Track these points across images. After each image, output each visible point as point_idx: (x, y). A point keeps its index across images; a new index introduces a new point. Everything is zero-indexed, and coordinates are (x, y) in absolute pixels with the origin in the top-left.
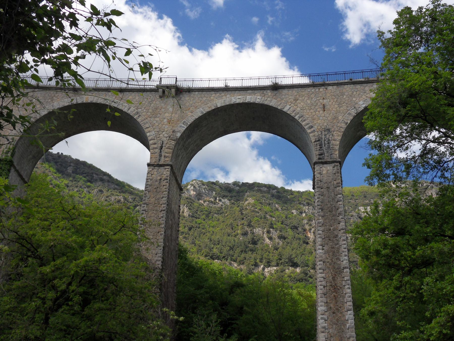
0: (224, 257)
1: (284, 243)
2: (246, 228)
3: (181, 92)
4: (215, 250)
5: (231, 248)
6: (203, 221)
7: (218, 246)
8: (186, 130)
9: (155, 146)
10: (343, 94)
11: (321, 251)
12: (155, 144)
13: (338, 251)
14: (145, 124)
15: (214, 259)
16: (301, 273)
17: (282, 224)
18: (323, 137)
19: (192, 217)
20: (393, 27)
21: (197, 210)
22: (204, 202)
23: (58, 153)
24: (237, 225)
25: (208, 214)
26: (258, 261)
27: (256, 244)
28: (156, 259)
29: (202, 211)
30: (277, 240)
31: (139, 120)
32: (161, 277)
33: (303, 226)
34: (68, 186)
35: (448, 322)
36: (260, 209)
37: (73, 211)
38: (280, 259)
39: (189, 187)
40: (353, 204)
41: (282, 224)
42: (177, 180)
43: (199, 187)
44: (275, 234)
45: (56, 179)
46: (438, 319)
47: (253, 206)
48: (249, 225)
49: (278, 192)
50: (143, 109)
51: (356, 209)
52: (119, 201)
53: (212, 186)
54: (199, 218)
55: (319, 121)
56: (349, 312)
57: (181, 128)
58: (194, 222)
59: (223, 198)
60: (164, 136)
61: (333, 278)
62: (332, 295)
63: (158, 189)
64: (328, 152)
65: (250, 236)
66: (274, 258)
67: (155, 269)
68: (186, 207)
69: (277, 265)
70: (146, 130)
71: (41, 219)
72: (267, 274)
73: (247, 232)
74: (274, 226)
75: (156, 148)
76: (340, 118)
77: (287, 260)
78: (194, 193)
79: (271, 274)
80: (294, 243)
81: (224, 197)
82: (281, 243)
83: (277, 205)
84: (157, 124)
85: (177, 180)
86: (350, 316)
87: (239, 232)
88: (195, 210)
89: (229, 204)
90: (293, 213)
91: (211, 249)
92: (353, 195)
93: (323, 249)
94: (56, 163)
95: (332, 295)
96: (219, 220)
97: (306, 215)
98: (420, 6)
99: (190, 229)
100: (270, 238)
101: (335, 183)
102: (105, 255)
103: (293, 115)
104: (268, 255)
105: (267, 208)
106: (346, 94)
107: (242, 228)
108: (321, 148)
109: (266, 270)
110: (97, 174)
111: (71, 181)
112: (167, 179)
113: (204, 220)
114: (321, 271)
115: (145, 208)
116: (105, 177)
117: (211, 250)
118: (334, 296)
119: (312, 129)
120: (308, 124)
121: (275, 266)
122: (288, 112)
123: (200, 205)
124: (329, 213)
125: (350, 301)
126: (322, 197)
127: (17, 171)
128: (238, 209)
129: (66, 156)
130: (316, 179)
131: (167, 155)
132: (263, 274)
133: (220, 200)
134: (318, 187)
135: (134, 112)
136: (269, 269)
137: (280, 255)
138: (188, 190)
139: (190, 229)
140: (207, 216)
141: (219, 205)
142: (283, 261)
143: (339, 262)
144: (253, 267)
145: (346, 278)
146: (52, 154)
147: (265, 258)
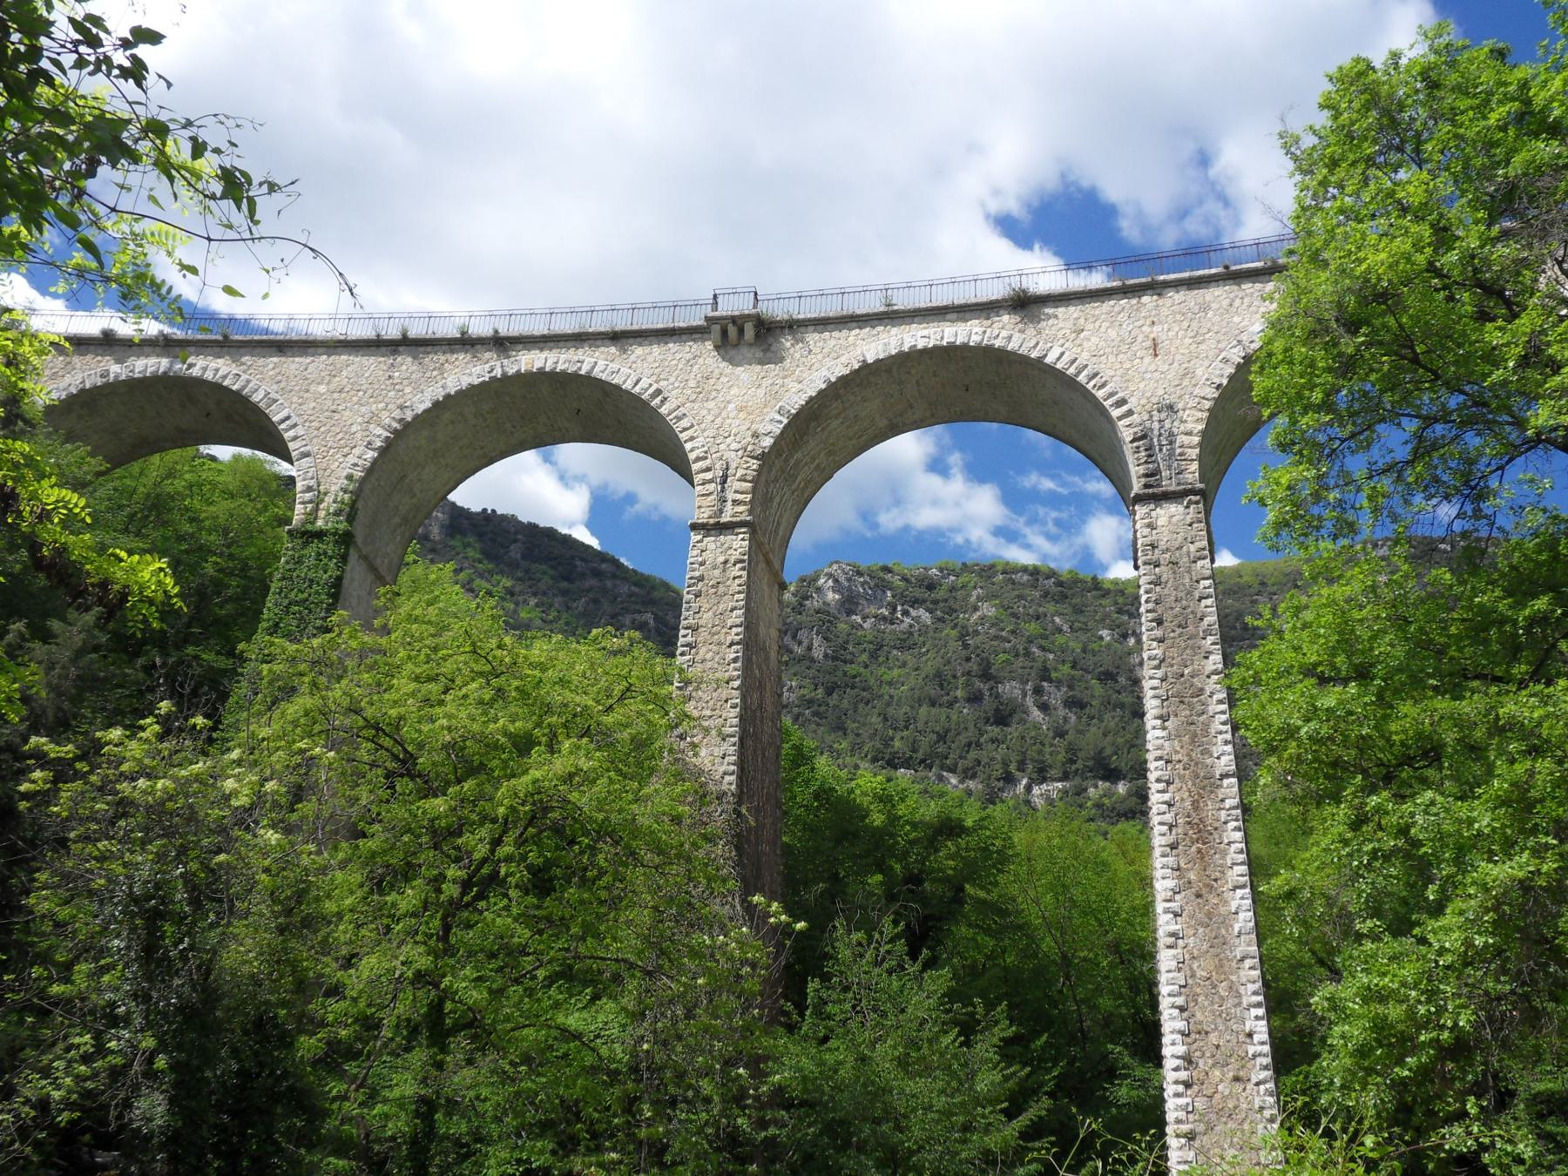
0: (923, 761)
1: (1080, 718)
2: (978, 684)
3: (769, 330)
4: (897, 744)
5: (942, 738)
7: (906, 733)
8: (786, 427)
9: (709, 476)
11: (1159, 733)
12: (708, 469)
13: (1206, 732)
14: (679, 419)
15: (896, 768)
16: (1129, 794)
17: (1073, 667)
19: (835, 659)
20: (1323, 119)
21: (847, 642)
22: (864, 618)
23: (485, 510)
24: (954, 677)
25: (877, 649)
26: (1013, 768)
27: (1007, 725)
28: (722, 769)
30: (1062, 712)
31: (663, 411)
32: (739, 814)
33: (1131, 671)
34: (512, 594)
35: (1487, 910)
36: (1013, 632)
37: (499, 653)
38: (1073, 762)
39: (822, 581)
41: (1073, 667)
42: (768, 563)
43: (849, 580)
44: (1056, 697)
45: (481, 576)
46: (1459, 904)
48: (986, 676)
49: (1060, 584)
50: (672, 379)
55: (1142, 385)
56: (1239, 892)
57: (771, 426)
58: (839, 673)
61: (1196, 805)
62: (1194, 849)
63: (721, 589)
64: (1169, 467)
65: (988, 704)
66: (1056, 754)
67: (721, 797)
69: (1065, 777)
70: (683, 436)
71: (417, 679)
72: (1039, 802)
73: (982, 694)
74: (1054, 675)
75: (711, 481)
76: (1199, 372)
77: (1091, 763)
79: (1050, 801)
80: (1107, 716)
81: (916, 603)
82: (1074, 718)
83: (1057, 620)
84: (710, 418)
85: (768, 563)
86: (1240, 901)
87: (959, 693)
90: (1101, 638)
91: (887, 742)
92: (1263, 584)
93: (1164, 729)
94: (480, 536)
95: (1194, 849)
96: (904, 665)
98: (1394, 48)
99: (829, 692)
100: (1044, 707)
101: (1192, 548)
102: (585, 765)
104: (1040, 752)
105: (1032, 628)
106: (1214, 306)
107: (967, 684)
108: (1150, 456)
109: (1036, 790)
110: (583, 560)
111: (519, 579)
112: (742, 561)
113: (866, 667)
114: (1161, 786)
115: (689, 639)
116: (604, 566)
117: (887, 745)
118: (1199, 851)
119: (1125, 408)
121: (1060, 780)
122: (1059, 366)
124: (1179, 631)
125: (1242, 863)
126: (1158, 589)
127: (365, 558)
128: (954, 633)
129: (504, 517)
130: (1139, 542)
131: (739, 497)
132: (1028, 802)
133: (906, 613)
134: (1145, 563)
135: (651, 391)
136: (1044, 787)
137: (1072, 750)
138: (819, 590)
139: (829, 692)
140: (874, 655)
141: (904, 626)
142: (1080, 765)
143: (1209, 761)
144: (1001, 784)
145: (1229, 803)
146: (459, 513)
147: (1032, 760)
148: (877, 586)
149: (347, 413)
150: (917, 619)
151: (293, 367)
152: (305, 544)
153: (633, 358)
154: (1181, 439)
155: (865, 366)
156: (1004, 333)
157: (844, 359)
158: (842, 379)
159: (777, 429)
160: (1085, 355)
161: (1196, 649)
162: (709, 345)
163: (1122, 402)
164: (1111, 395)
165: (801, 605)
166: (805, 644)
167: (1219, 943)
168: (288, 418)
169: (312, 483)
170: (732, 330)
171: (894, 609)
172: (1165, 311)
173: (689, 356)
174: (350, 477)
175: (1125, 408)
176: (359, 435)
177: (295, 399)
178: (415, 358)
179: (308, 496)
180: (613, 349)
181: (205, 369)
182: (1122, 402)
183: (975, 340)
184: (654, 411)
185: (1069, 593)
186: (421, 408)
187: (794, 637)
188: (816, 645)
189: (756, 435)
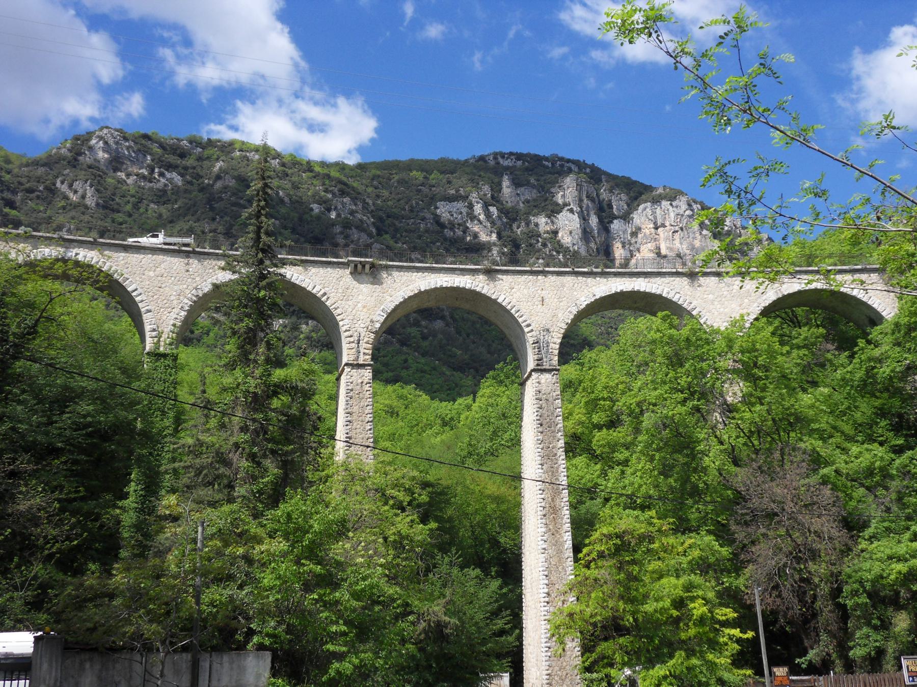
6: (127, 219)
9: (352, 339)
10: (563, 286)
12: (351, 336)
18: (542, 338)
21: (114, 194)
22: (128, 175)
29: (124, 196)
31: (328, 303)
33: (333, 238)
40: (426, 196)
43: (117, 143)
47: (234, 194)
49: (283, 165)
51: (430, 205)
53: (143, 142)
54: (119, 212)
59: (167, 170)
61: (553, 499)
68: (91, 186)
70: (338, 318)
76: (560, 315)
78: (106, 156)
81: (170, 167)
88: (109, 193)
89: (180, 183)
90: (312, 210)
97: (338, 215)
103: (509, 307)
119: (530, 328)
120: (525, 321)
123: (119, 182)
131: (367, 351)
133: (161, 175)
138: (91, 148)
141: (160, 185)
148: (139, 150)
149: (167, 289)
150: (170, 180)
151: (134, 259)
152: (157, 361)
153: (310, 273)
154: (552, 345)
155: (420, 293)
156: (481, 285)
157: (410, 287)
158: (410, 297)
159: (382, 319)
160: (514, 300)
161: (554, 437)
162: (348, 271)
163: (529, 325)
164: (525, 321)
165: (76, 160)
166: (80, 193)
167: (560, 552)
168: (136, 290)
169: (155, 327)
170: (359, 266)
171: (152, 171)
172: (547, 285)
173: (338, 276)
174: (174, 325)
175: (530, 328)
176: (175, 302)
177: (138, 279)
178: (199, 261)
179: (154, 334)
180: (300, 268)
181: (77, 254)
182: (529, 325)
183: (468, 286)
184: (323, 303)
185: (290, 172)
186: (206, 290)
187: (70, 186)
188: (89, 195)
189: (372, 321)
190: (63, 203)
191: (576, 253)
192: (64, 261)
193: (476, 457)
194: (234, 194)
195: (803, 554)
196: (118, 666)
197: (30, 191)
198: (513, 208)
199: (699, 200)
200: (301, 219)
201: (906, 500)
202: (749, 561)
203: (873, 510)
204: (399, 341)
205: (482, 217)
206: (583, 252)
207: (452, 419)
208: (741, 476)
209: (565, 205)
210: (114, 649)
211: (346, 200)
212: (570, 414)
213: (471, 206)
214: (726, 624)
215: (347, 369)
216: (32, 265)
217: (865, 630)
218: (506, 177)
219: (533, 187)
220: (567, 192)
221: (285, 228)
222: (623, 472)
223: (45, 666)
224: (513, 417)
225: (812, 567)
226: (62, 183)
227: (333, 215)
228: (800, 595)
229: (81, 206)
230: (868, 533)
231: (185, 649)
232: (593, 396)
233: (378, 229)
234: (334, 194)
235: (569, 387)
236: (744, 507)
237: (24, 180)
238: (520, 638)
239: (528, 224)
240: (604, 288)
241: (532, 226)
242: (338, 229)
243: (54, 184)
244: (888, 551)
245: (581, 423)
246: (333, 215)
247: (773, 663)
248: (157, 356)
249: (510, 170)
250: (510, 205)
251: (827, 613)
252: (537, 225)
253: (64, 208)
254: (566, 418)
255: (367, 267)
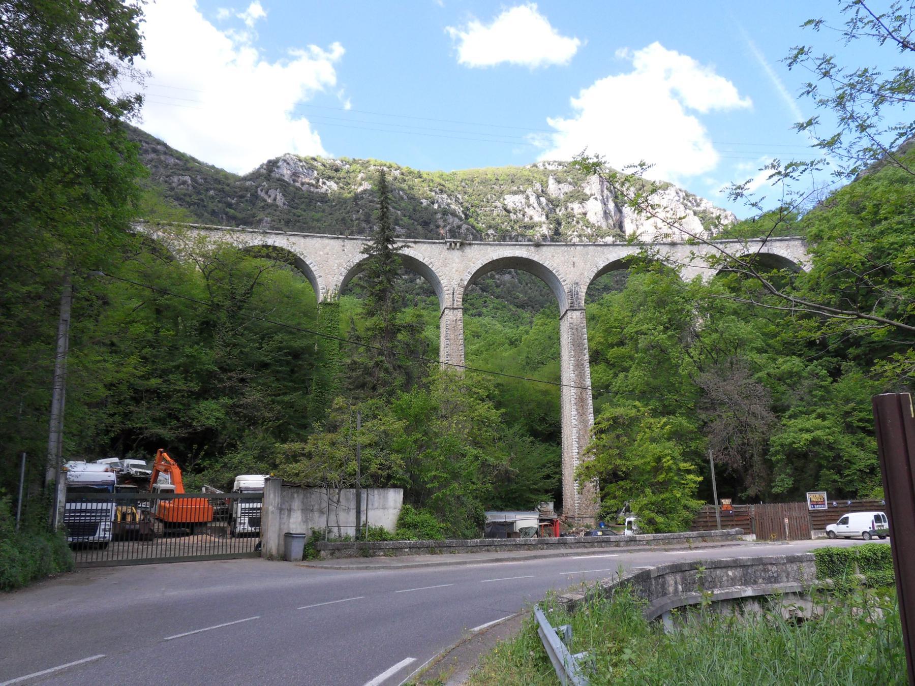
10: (588, 254)
43: (295, 164)
47: (370, 195)
49: (402, 174)
51: (500, 197)
52: (184, 183)
60: (455, 283)
81: (329, 178)
86: (591, 417)
89: (336, 189)
92: (497, 179)
96: (324, 211)
97: (439, 206)
110: (147, 143)
116: (159, 147)
133: (324, 183)
140: (308, 205)
150: (329, 187)
162: (445, 248)
163: (564, 281)
166: (272, 197)
182: (564, 281)
188: (278, 198)
190: (262, 204)
191: (599, 228)
192: (267, 247)
193: (532, 365)
194: (370, 195)
195: (743, 427)
196: (313, 496)
197: (242, 197)
198: (556, 198)
199: (683, 189)
200: (414, 210)
201: (814, 393)
202: (709, 432)
203: (793, 400)
204: (481, 288)
205: (536, 205)
206: (604, 226)
207: (516, 340)
208: (706, 379)
209: (592, 195)
210: (309, 486)
211: (445, 196)
212: (593, 337)
213: (527, 198)
214: (689, 472)
215: (447, 311)
216: (248, 251)
217: (783, 476)
218: (551, 177)
219: (570, 183)
220: (593, 186)
221: (405, 216)
222: (626, 376)
223: (272, 496)
224: (554, 339)
225: (750, 435)
226: (262, 190)
227: (436, 206)
228: (742, 453)
229: (274, 206)
230: (787, 414)
231: (352, 486)
232: (608, 326)
233: (466, 215)
234: (436, 193)
235: (592, 319)
236: (706, 398)
237: (238, 190)
238: (560, 481)
239: (566, 209)
240: (615, 255)
241: (569, 210)
242: (439, 216)
243: (256, 192)
244: (800, 426)
245: (600, 343)
246: (436, 206)
247: (721, 496)
248: (325, 304)
249: (554, 173)
250: (554, 196)
251: (758, 466)
252: (572, 209)
253: (263, 207)
254: (590, 340)
255: (458, 245)
